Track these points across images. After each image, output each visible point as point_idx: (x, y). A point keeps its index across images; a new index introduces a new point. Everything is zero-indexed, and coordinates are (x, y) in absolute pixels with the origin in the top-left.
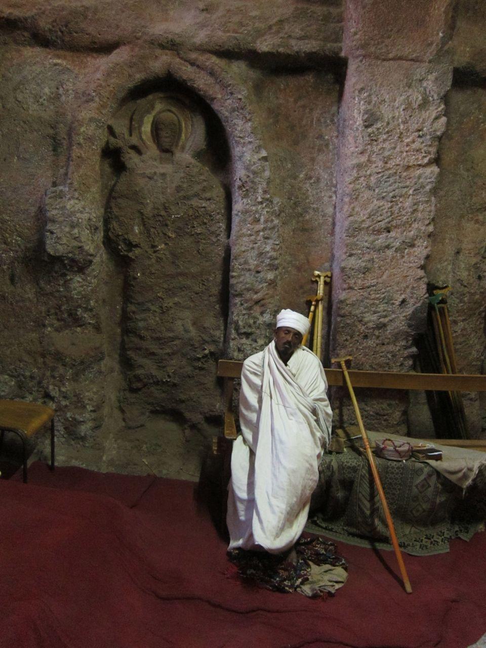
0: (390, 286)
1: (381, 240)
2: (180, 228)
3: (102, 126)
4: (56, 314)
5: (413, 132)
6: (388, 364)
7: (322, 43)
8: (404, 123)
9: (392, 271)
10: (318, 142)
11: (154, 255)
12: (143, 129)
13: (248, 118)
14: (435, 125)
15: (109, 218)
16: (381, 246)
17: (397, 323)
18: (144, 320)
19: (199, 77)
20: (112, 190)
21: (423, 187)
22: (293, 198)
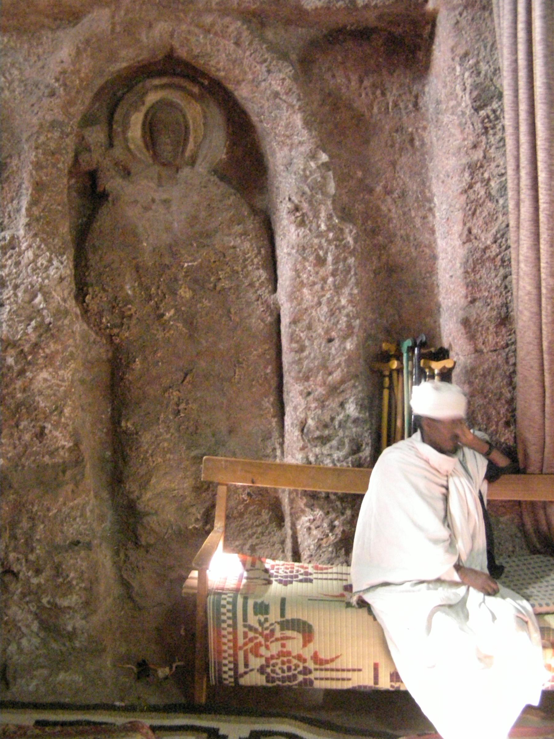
12: (130, 134)
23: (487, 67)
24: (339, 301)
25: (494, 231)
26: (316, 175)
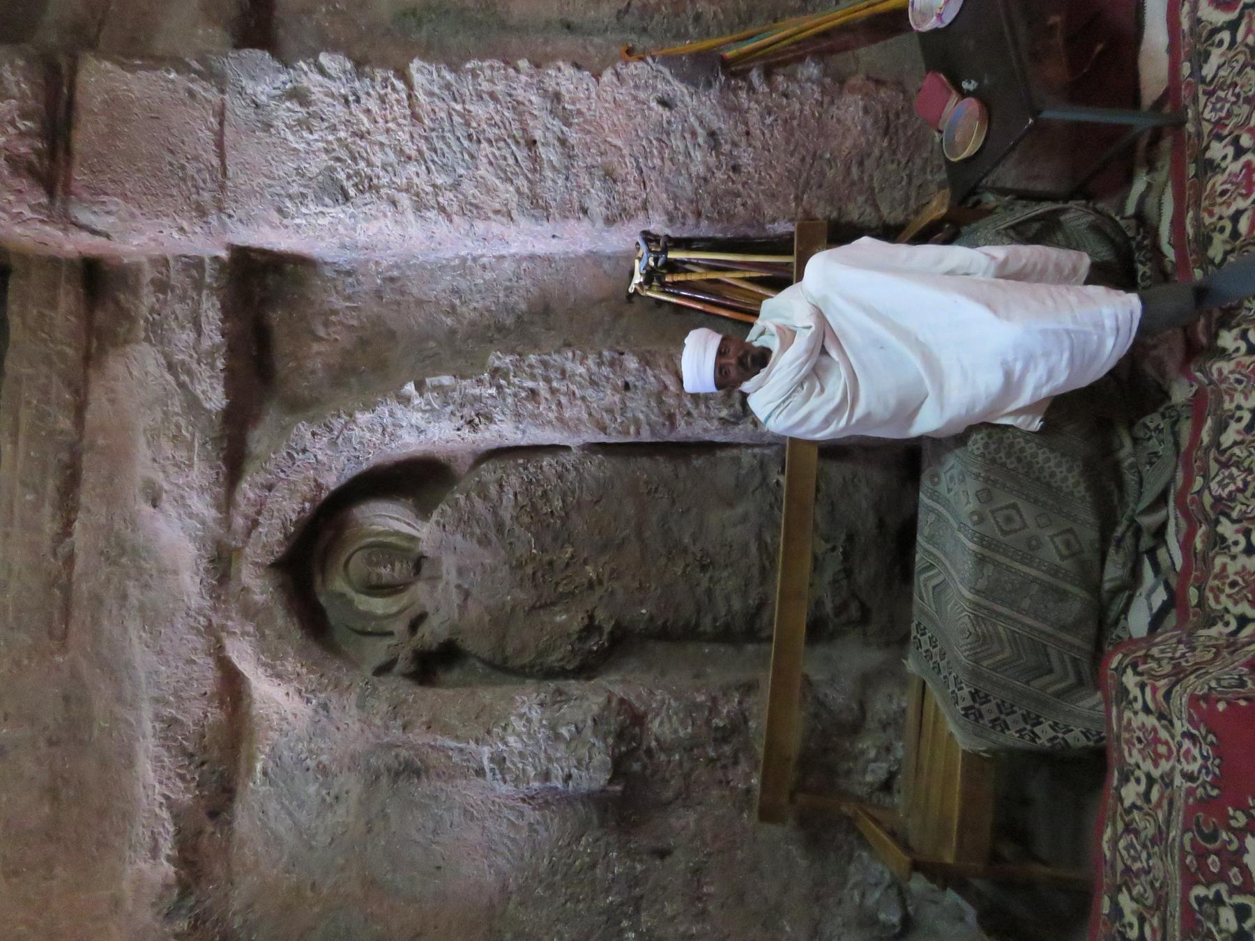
0: (636, 131)
1: (550, 154)
2: (555, 539)
3: (373, 685)
4: (724, 767)
5: (351, 113)
6: (785, 121)
7: (205, 292)
8: (333, 129)
9: (607, 130)
10: (388, 296)
11: (605, 584)
12: (380, 612)
13: (347, 418)
14: (332, 72)
15: (541, 670)
16: (562, 154)
17: (706, 112)
18: (727, 598)
19: (279, 510)
20: (490, 664)
21: (448, 86)
22: (490, 334)
23: (294, 184)
24: (581, 375)
25: (497, 182)
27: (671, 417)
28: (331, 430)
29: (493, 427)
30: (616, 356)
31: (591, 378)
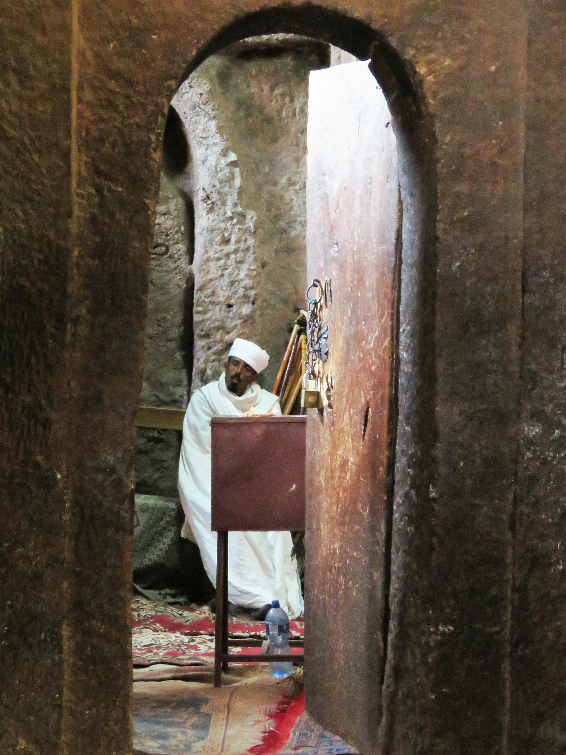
13: (212, 116)
24: (238, 274)
26: (225, 171)
27: (207, 336)
28: (204, 105)
29: (204, 213)
30: (252, 299)
31: (236, 281)
